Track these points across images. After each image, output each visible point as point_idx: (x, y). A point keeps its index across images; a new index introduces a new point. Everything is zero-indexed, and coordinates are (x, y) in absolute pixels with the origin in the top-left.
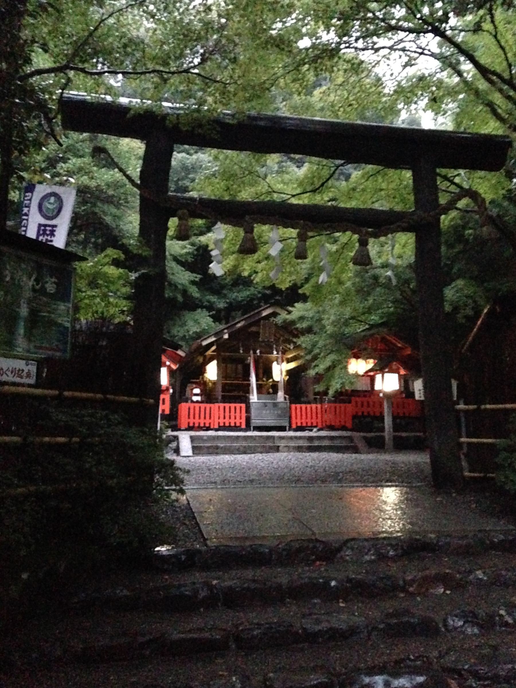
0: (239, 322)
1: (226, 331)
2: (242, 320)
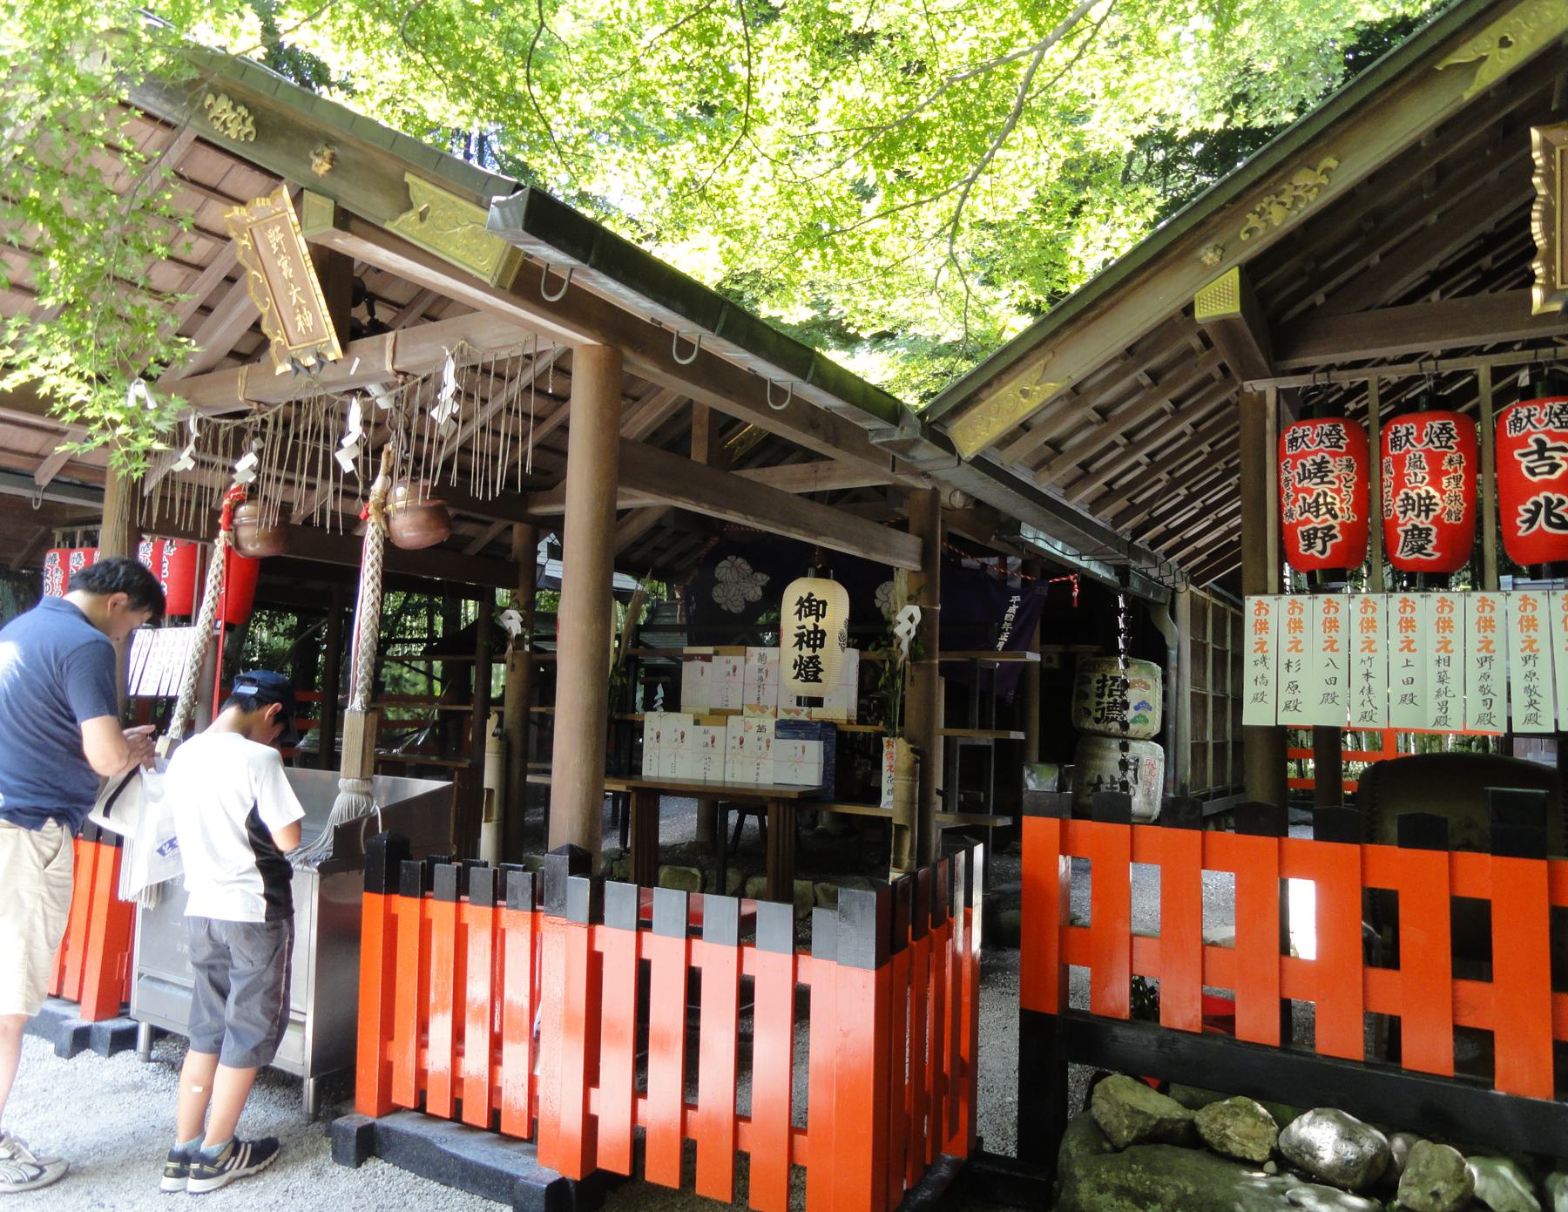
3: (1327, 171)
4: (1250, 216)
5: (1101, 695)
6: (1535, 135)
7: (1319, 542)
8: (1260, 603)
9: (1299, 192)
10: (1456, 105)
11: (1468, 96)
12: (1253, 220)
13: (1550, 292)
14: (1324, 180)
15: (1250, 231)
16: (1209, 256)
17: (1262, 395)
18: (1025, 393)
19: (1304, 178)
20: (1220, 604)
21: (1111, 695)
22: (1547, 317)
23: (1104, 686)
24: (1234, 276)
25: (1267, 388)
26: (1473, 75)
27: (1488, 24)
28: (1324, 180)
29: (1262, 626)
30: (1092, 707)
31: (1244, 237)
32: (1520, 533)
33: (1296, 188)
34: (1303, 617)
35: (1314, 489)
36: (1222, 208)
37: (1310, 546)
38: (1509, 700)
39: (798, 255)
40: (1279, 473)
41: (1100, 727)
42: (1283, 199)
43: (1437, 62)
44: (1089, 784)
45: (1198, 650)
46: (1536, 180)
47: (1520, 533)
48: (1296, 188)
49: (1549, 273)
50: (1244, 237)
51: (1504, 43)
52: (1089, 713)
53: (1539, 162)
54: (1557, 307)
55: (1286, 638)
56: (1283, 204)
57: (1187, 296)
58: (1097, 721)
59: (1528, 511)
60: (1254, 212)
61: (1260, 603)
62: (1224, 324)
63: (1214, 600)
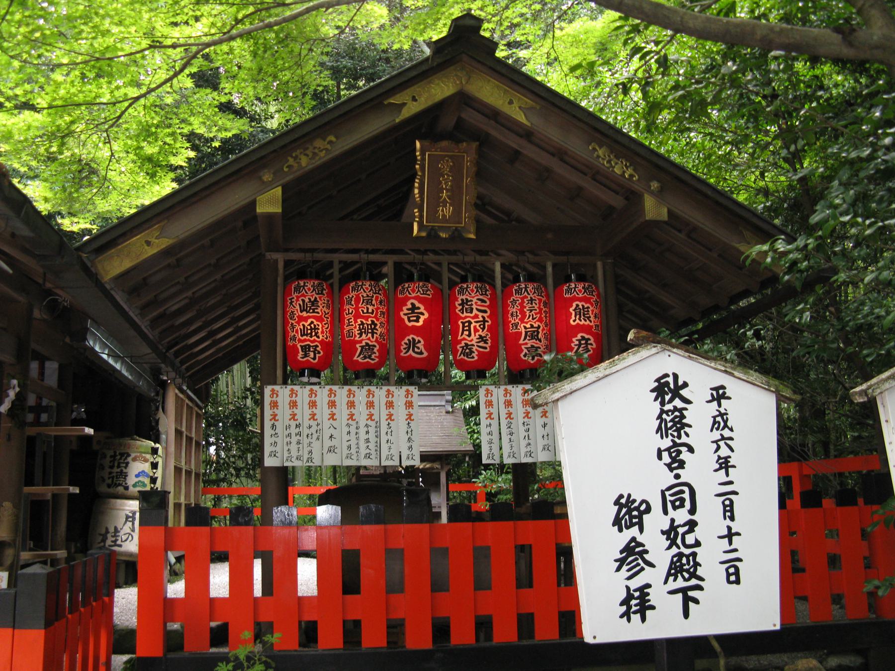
3: (330, 142)
4: (290, 158)
5: (112, 467)
6: (418, 144)
7: (312, 354)
8: (273, 390)
9: (316, 151)
10: (392, 123)
11: (397, 121)
12: (291, 161)
13: (421, 227)
14: (329, 147)
15: (289, 167)
16: (267, 177)
17: (276, 261)
18: (148, 243)
19: (319, 143)
20: (190, 404)
21: (119, 467)
22: (418, 238)
23: (115, 460)
24: (278, 191)
25: (280, 258)
26: (400, 111)
27: (407, 88)
28: (329, 147)
29: (274, 405)
30: (106, 476)
31: (286, 169)
32: (402, 354)
33: (315, 148)
34: (317, 399)
35: (306, 319)
36: (275, 151)
37: (306, 355)
38: (500, 439)
39: (264, 94)
40: (285, 307)
41: (111, 490)
42: (308, 152)
43: (386, 99)
44: (101, 535)
45: (178, 433)
46: (417, 166)
47: (402, 354)
48: (315, 148)
49: (421, 216)
50: (286, 169)
51: (414, 99)
52: (104, 480)
53: (419, 158)
54: (424, 234)
55: (307, 412)
56: (307, 155)
57: (253, 198)
58: (109, 486)
59: (406, 344)
60: (292, 157)
61: (273, 390)
62: (270, 217)
63: (187, 401)
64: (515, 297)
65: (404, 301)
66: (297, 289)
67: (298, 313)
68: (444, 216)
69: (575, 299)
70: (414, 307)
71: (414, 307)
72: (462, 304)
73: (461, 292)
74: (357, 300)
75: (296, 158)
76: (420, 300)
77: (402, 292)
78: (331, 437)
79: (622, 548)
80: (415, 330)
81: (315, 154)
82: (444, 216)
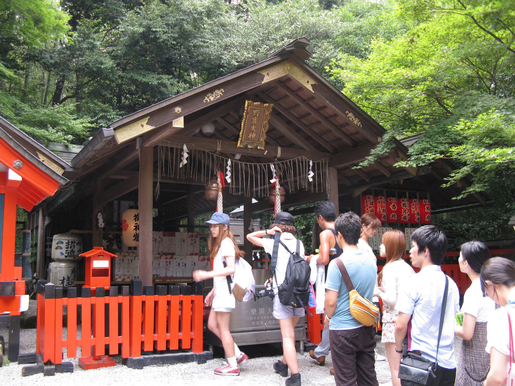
0: (211, 90)
1: (178, 110)
2: (218, 87)
54: (242, 146)
64: (414, 203)
65: (391, 203)
66: (368, 198)
67: (369, 205)
68: (251, 137)
69: (427, 204)
70: (394, 205)
71: (394, 205)
72: (404, 204)
73: (403, 201)
74: (382, 202)
75: (208, 97)
76: (396, 203)
77: (390, 200)
78: (185, 265)
79: (66, 375)
80: (394, 212)
81: (216, 96)
82: (251, 137)
